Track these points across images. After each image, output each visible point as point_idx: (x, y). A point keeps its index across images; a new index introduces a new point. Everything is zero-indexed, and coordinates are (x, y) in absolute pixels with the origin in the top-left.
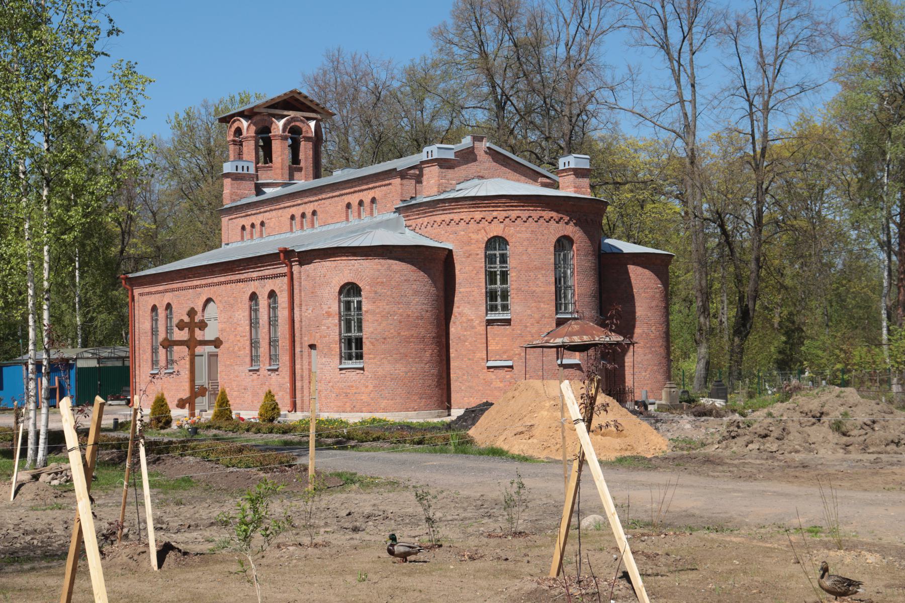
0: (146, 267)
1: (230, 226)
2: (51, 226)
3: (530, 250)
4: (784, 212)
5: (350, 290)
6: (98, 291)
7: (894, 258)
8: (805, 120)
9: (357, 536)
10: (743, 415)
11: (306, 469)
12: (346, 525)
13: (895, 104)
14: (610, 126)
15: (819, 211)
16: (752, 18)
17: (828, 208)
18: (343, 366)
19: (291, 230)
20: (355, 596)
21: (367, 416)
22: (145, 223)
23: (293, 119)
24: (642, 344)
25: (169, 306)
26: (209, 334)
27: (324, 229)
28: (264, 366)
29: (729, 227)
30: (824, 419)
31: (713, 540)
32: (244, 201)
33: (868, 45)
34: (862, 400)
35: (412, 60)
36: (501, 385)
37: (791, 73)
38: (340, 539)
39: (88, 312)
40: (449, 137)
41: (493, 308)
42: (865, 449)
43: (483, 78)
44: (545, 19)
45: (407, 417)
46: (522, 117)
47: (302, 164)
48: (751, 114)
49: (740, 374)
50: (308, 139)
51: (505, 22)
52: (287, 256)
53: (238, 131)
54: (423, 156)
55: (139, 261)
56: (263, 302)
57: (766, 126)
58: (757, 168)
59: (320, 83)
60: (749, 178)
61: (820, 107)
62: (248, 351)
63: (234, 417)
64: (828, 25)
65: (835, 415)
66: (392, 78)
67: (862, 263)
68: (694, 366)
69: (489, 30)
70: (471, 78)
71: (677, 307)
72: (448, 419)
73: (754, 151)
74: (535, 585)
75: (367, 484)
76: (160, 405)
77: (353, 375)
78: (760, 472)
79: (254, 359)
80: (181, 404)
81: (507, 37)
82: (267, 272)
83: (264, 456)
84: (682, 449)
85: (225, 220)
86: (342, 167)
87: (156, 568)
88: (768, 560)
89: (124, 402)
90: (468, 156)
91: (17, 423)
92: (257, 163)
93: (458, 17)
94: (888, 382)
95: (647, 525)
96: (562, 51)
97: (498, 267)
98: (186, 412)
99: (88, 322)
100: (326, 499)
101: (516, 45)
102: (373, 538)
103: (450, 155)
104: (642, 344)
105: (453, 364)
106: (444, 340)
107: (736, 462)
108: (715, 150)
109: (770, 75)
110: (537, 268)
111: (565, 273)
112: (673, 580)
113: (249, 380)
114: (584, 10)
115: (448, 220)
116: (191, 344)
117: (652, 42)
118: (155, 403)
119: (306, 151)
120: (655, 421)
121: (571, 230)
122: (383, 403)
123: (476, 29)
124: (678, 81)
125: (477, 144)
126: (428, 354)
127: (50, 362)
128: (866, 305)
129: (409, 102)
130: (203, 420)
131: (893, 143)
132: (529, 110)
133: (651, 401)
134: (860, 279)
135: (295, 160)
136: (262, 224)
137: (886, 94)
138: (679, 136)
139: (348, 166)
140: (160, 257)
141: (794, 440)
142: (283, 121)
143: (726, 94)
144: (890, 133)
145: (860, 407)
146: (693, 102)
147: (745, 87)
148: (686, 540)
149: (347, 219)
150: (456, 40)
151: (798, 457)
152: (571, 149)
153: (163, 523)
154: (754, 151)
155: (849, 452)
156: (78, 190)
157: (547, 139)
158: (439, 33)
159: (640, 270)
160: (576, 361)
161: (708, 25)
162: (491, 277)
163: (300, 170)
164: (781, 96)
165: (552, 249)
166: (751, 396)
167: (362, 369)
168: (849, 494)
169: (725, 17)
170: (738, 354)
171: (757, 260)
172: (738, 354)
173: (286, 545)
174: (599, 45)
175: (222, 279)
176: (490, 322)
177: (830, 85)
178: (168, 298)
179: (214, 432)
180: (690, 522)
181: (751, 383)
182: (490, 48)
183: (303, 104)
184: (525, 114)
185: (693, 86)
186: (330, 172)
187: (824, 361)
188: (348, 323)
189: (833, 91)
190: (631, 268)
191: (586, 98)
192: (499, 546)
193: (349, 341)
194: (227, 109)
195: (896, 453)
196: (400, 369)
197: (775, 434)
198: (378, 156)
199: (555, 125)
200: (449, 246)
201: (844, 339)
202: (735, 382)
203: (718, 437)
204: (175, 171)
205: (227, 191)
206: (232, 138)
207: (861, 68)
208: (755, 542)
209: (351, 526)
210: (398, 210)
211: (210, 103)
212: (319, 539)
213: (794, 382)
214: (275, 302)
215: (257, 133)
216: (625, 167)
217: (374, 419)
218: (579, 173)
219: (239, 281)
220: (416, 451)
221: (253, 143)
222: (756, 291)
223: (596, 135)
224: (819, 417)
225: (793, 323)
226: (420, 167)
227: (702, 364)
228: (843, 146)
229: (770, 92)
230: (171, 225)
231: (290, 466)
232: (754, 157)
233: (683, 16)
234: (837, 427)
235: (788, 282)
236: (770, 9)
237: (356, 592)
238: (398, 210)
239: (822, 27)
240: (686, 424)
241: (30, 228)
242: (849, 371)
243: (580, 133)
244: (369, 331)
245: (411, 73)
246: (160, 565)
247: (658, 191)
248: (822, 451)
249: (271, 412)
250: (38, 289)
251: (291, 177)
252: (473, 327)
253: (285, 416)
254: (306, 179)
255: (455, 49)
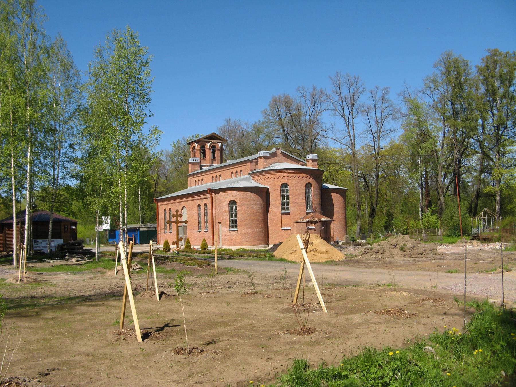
0: (164, 195)
1: (191, 180)
2: (127, 182)
3: (296, 188)
4: (386, 174)
5: (233, 202)
6: (146, 204)
7: (423, 189)
8: (392, 142)
9: (230, 290)
10: (371, 245)
11: (214, 266)
12: (226, 286)
13: (422, 137)
14: (325, 144)
15: (398, 174)
16: (373, 106)
17: (401, 172)
18: (230, 230)
19: (212, 182)
20: (224, 310)
21: (239, 247)
22: (163, 180)
23: (213, 143)
24: (336, 221)
25: (170, 209)
26: (184, 218)
27: (224, 181)
28: (203, 230)
29: (367, 179)
30: (397, 246)
31: (354, 290)
32: (196, 172)
33: (412, 117)
34: (410, 239)
35: (255, 122)
36: (287, 236)
37: (388, 125)
38: (224, 291)
39: (143, 211)
40: (268, 148)
41: (284, 209)
42: (411, 257)
43: (281, 128)
44: (301, 107)
45: (253, 248)
46: (294, 141)
47: (216, 158)
48: (374, 140)
49: (371, 231)
50: (218, 150)
51: (288, 108)
52: (210, 191)
53: (194, 147)
54: (258, 155)
55: (161, 194)
56: (202, 207)
57: (379, 144)
58: (376, 158)
59: (223, 130)
60: (374, 162)
61: (397, 137)
62: (197, 225)
63: (192, 248)
64: (398, 109)
65: (401, 245)
66: (248, 128)
67: (413, 191)
68: (356, 228)
69: (282, 111)
70: (276, 128)
71: (350, 208)
72: (267, 248)
73: (375, 152)
74: (287, 306)
75: (236, 272)
76: (166, 244)
77: (234, 233)
78: (374, 265)
79: (199, 227)
80: (174, 243)
81: (288, 113)
82: (203, 197)
83: (200, 262)
84: (349, 258)
85: (189, 178)
86: (231, 160)
87: (158, 300)
88: (371, 296)
89: (155, 243)
90: (274, 155)
91: (116, 250)
92: (200, 158)
93: (271, 106)
94: (421, 233)
95: (332, 285)
96: (307, 118)
97: (285, 194)
98: (175, 246)
99: (144, 215)
100: (220, 277)
101: (291, 116)
102: (235, 291)
103: (268, 155)
104: (336, 221)
105: (269, 229)
106: (266, 220)
107: (367, 262)
108: (362, 152)
109: (380, 126)
110: (299, 194)
111: (309, 196)
112: (337, 304)
113: (197, 235)
114: (315, 103)
115: (267, 178)
116: (177, 222)
117: (339, 115)
118: (165, 243)
119: (217, 154)
120: (340, 248)
121: (311, 181)
122: (245, 243)
123: (277, 111)
124: (348, 128)
125: (277, 150)
126: (260, 225)
127: (127, 229)
128: (415, 206)
129: (255, 136)
130: (181, 249)
131: (422, 150)
132: (297, 138)
133: (340, 241)
134: (412, 197)
135: (214, 157)
136: (202, 180)
137: (419, 133)
138: (349, 147)
139: (233, 159)
140: (168, 191)
141: (387, 253)
142: (209, 144)
143: (365, 132)
144: (420, 147)
145: (409, 242)
146: (354, 135)
147: (371, 130)
148: (344, 290)
149: (232, 178)
150: (270, 114)
151: (388, 260)
152: (311, 152)
153: (163, 285)
154: (375, 152)
155: (405, 258)
156: (137, 169)
157: (303, 148)
158: (264, 112)
159: (335, 194)
160: (313, 227)
161: (358, 109)
162: (283, 197)
163: (215, 160)
164: (384, 133)
165: (304, 187)
166: (375, 238)
167: (237, 231)
168: (402, 272)
169: (364, 106)
170: (371, 224)
171: (377, 190)
172: (371, 224)
173: (203, 293)
174: (321, 115)
175: (188, 199)
176: (282, 214)
177: (400, 130)
178: (170, 206)
179: (185, 253)
180: (348, 283)
181: (375, 234)
182: (283, 117)
183: (216, 137)
184: (295, 140)
185: (353, 130)
186: (226, 161)
187: (400, 226)
188: (232, 214)
189: (401, 132)
190: (332, 194)
191: (317, 134)
192: (278, 293)
193: (233, 221)
194: (191, 140)
195: (421, 257)
196: (250, 231)
197: (381, 252)
198: (243, 155)
199: (306, 144)
200: (268, 187)
201: (407, 218)
202: (370, 234)
203: (361, 253)
204: (173, 162)
205: (190, 169)
206: (192, 150)
207: (410, 124)
208: (368, 290)
209: (228, 286)
210: (249, 174)
211: (185, 138)
212: (215, 291)
213: (390, 233)
214: (207, 207)
215: (200, 148)
216: (331, 158)
217: (241, 249)
218: (313, 160)
219: (194, 200)
220: (255, 260)
221: (199, 151)
222: (377, 201)
223: (321, 147)
224: (396, 246)
225: (390, 212)
226: (257, 159)
227: (359, 228)
228: (405, 151)
229: (380, 132)
230: (172, 180)
231: (209, 265)
232: (375, 155)
233: (349, 106)
234: (402, 249)
235: (388, 198)
236: (379, 104)
237: (225, 309)
238: (249, 174)
239: (396, 110)
240: (351, 249)
241: (121, 183)
242: (409, 229)
243: (315, 146)
244: (240, 217)
245: (255, 127)
246: (160, 299)
247: (343, 166)
248: (397, 257)
249: (205, 246)
250: (123, 204)
251: (212, 163)
252: (276, 216)
253: (210, 247)
254: (218, 163)
255: (270, 118)
